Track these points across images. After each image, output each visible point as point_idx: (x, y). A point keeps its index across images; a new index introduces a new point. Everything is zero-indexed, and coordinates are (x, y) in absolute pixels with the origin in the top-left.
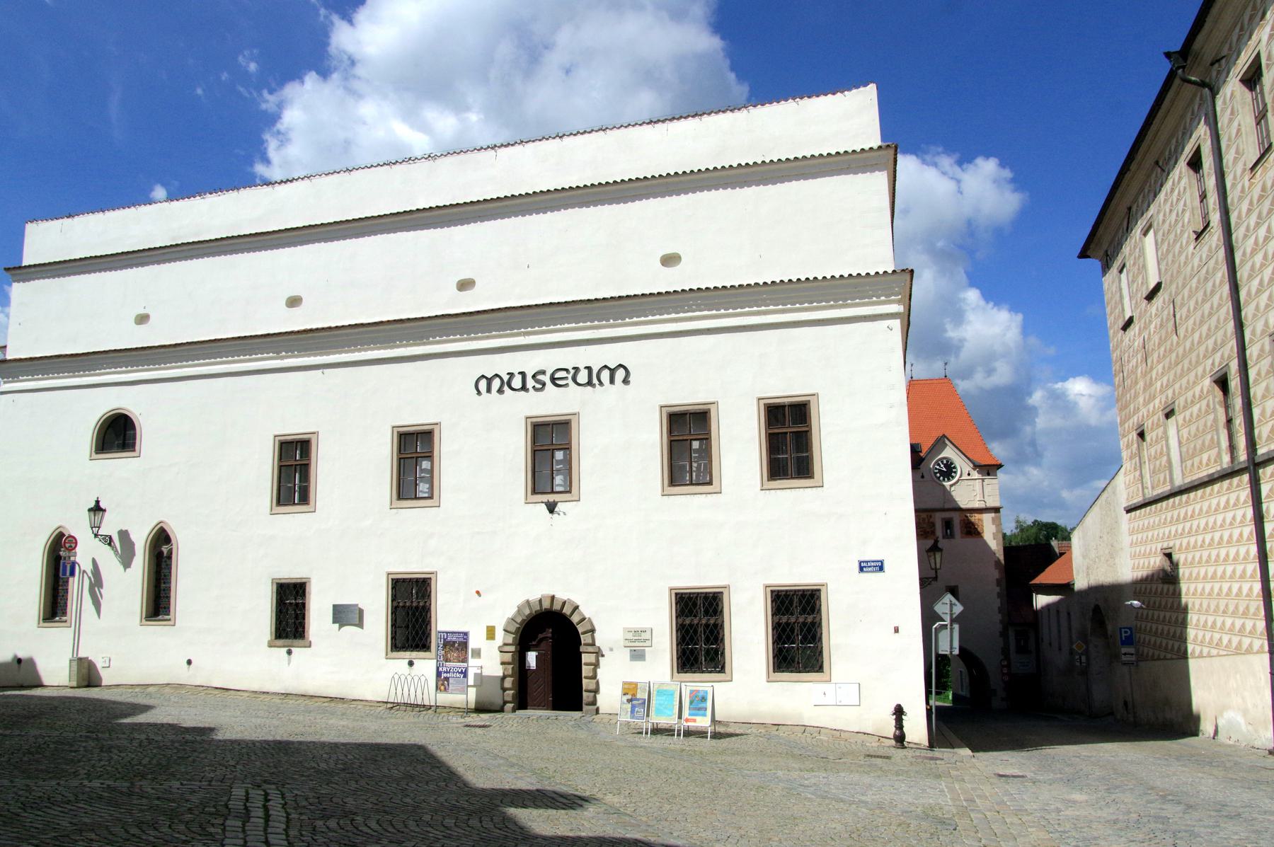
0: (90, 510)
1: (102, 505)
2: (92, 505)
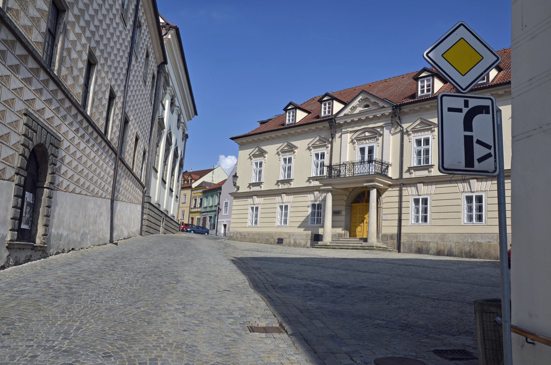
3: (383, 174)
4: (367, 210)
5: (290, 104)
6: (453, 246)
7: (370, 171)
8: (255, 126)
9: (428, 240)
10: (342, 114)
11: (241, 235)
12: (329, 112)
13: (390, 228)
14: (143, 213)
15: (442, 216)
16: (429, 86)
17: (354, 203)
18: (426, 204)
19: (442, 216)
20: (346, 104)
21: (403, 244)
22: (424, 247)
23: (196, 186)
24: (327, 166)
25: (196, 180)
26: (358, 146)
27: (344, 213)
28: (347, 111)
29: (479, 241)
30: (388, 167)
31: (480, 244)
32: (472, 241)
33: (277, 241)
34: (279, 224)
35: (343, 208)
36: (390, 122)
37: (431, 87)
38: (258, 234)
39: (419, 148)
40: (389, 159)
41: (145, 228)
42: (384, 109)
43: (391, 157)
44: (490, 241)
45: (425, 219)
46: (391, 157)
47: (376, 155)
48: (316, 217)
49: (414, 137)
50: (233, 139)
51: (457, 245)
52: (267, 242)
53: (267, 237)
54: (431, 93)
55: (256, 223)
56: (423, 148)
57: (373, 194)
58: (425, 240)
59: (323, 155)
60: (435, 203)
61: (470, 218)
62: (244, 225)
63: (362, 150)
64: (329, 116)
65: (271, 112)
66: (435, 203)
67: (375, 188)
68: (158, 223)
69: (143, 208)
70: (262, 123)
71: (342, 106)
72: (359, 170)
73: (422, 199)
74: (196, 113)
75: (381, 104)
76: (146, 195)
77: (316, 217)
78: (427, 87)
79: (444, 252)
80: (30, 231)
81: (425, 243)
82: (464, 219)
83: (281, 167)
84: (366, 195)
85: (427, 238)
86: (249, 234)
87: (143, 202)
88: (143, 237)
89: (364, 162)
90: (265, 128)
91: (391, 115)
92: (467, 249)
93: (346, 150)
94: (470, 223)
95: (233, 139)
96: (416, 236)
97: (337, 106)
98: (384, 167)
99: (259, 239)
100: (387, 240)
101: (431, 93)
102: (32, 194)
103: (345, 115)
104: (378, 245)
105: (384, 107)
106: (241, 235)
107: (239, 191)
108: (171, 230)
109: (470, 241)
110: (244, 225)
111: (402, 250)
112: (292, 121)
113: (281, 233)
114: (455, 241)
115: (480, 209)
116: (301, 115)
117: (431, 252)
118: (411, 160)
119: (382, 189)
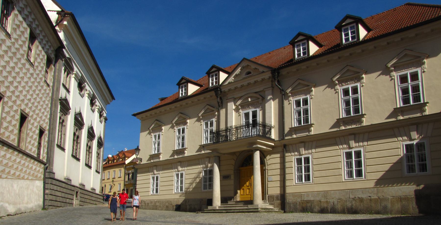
3: (266, 135)
4: (251, 173)
5: (182, 79)
6: (336, 203)
7: (253, 134)
8: (158, 102)
9: (312, 199)
10: (227, 83)
11: (145, 204)
13: (274, 189)
14: (45, 189)
15: (324, 173)
16: (305, 49)
17: (242, 166)
18: (308, 162)
19: (324, 173)
20: (229, 74)
21: (289, 203)
22: (309, 205)
23: (128, 162)
25: (129, 158)
26: (242, 112)
27: (232, 177)
28: (231, 79)
29: (360, 196)
30: (270, 129)
31: (361, 200)
32: (353, 197)
33: (175, 207)
34: (152, 193)
35: (231, 172)
36: (270, 85)
38: (159, 201)
40: (271, 122)
41: (47, 203)
42: (264, 74)
43: (273, 120)
44: (370, 195)
45: (308, 178)
46: (273, 120)
47: (260, 119)
49: (293, 100)
50: (134, 115)
51: (340, 202)
52: (167, 208)
53: (167, 204)
54: (306, 55)
55: (157, 192)
57: (257, 156)
58: (309, 199)
60: (315, 162)
61: (350, 174)
62: (169, 192)
63: (247, 115)
65: (170, 91)
66: (315, 162)
67: (257, 150)
68: (70, 196)
69: (45, 183)
71: (227, 75)
72: (243, 133)
73: (305, 158)
74: (113, 98)
76: (48, 171)
78: (303, 50)
79: (328, 210)
80: (106, 196)
81: (308, 202)
82: (344, 176)
83: (176, 138)
85: (310, 196)
86: (151, 202)
87: (45, 178)
88: (47, 211)
91: (271, 79)
92: (349, 205)
93: (233, 117)
95: (134, 115)
96: (300, 195)
97: (223, 76)
98: (267, 130)
99: (160, 207)
100: (273, 201)
101: (306, 55)
102: (138, 175)
103: (229, 83)
104: (264, 207)
105: (263, 72)
106: (145, 204)
107: (142, 163)
108: (88, 201)
109: (352, 196)
110: (169, 192)
111: (287, 209)
112: (185, 94)
114: (337, 197)
115: (359, 164)
117: (315, 210)
118: (291, 121)
119: (265, 151)
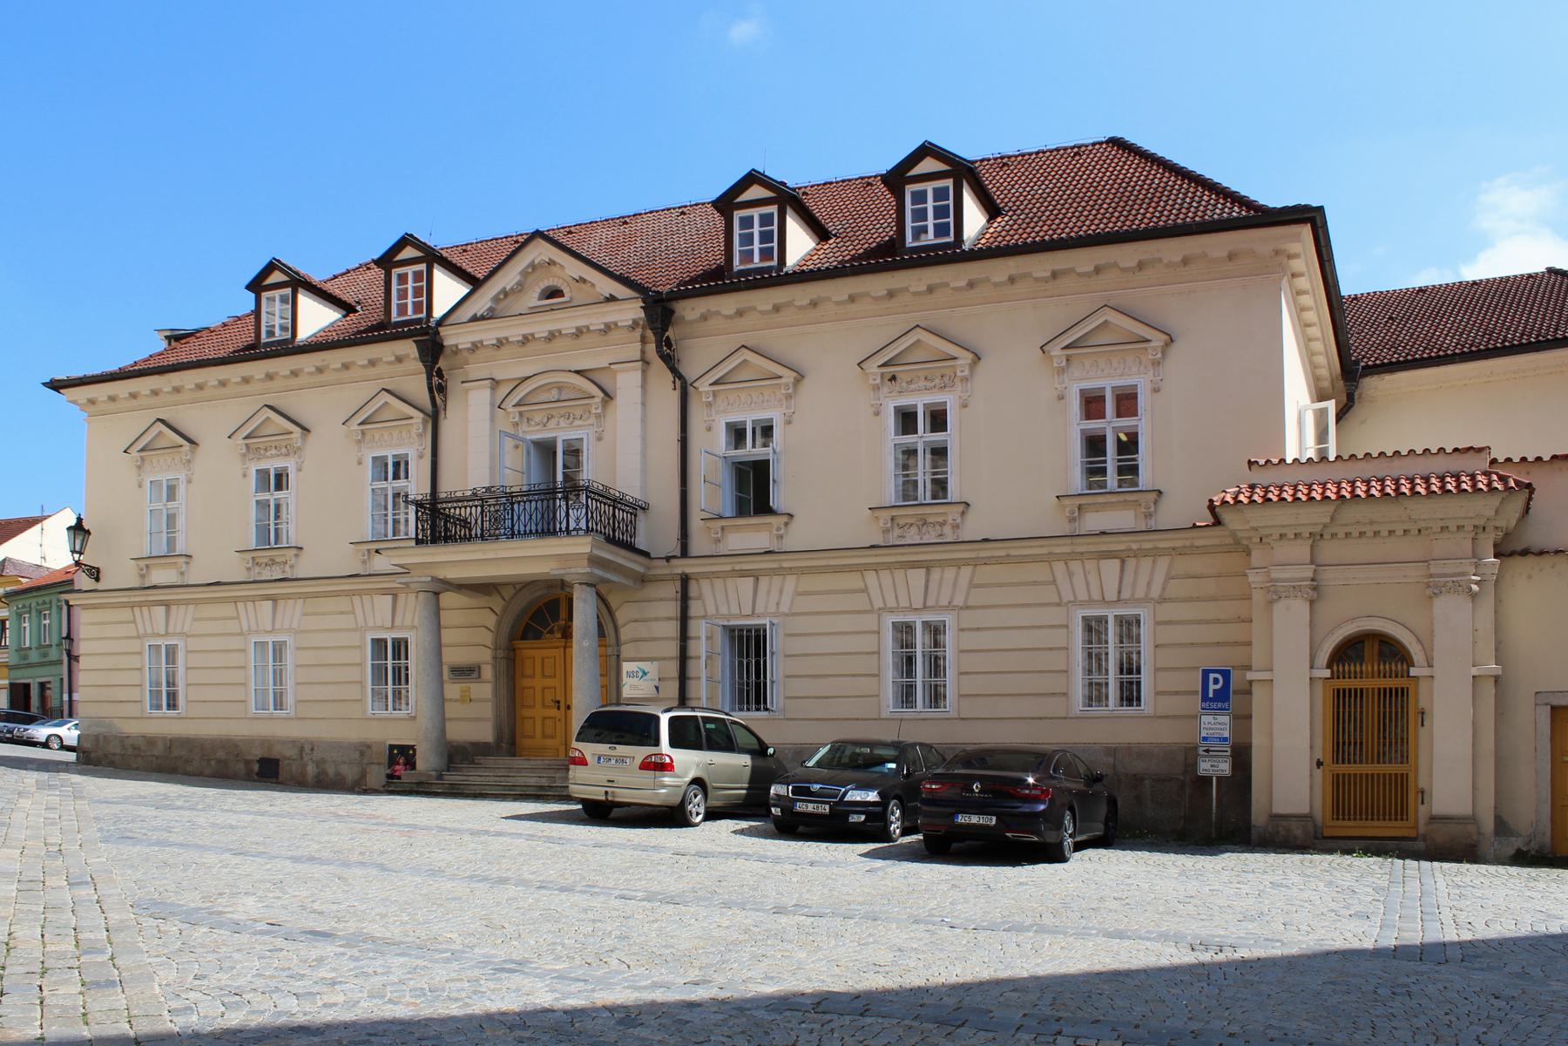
0: (69, 529)
1: (86, 525)
2: (73, 522)
5: (271, 267)
12: (417, 307)
17: (524, 637)
20: (475, 283)
24: (419, 505)
27: (487, 672)
33: (256, 767)
37: (775, 228)
39: (909, 439)
42: (612, 306)
48: (390, 662)
50: (56, 386)
53: (221, 754)
56: (923, 437)
59: (400, 468)
64: (419, 321)
70: (176, 338)
71: (462, 289)
72: (1423, 810)
75: (607, 286)
77: (390, 662)
84: (563, 614)
89: (554, 491)
90: (185, 353)
94: (907, 713)
95: (56, 386)
105: (612, 299)
113: (267, 742)
116: (314, 317)
